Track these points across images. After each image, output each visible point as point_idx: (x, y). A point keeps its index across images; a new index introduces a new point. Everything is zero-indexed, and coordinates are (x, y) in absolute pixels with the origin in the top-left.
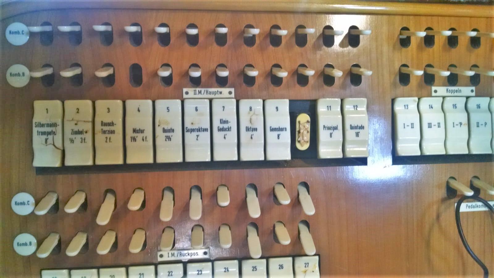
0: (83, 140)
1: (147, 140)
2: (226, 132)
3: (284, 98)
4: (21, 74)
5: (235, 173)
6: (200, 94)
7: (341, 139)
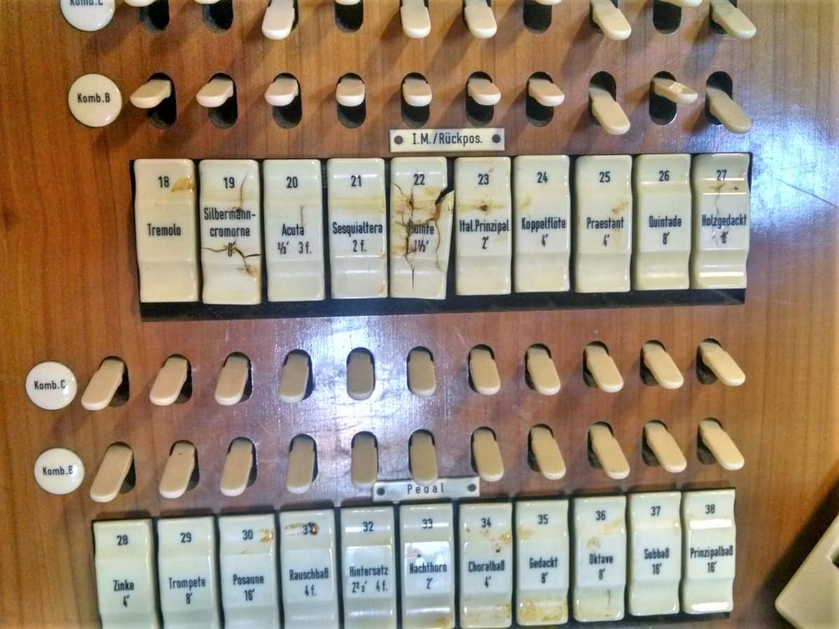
0: (304, 248)
1: (309, 251)
4: (103, 98)
5: (506, 320)
6: (425, 143)
7: (688, 248)
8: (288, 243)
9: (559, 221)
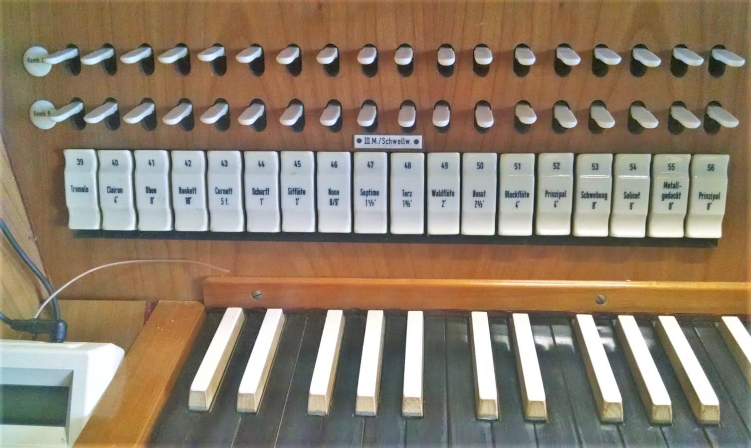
2: (673, 199)
3: (344, 151)
6: (374, 144)
7: (685, 213)
8: (483, 201)
9: (451, 192)
